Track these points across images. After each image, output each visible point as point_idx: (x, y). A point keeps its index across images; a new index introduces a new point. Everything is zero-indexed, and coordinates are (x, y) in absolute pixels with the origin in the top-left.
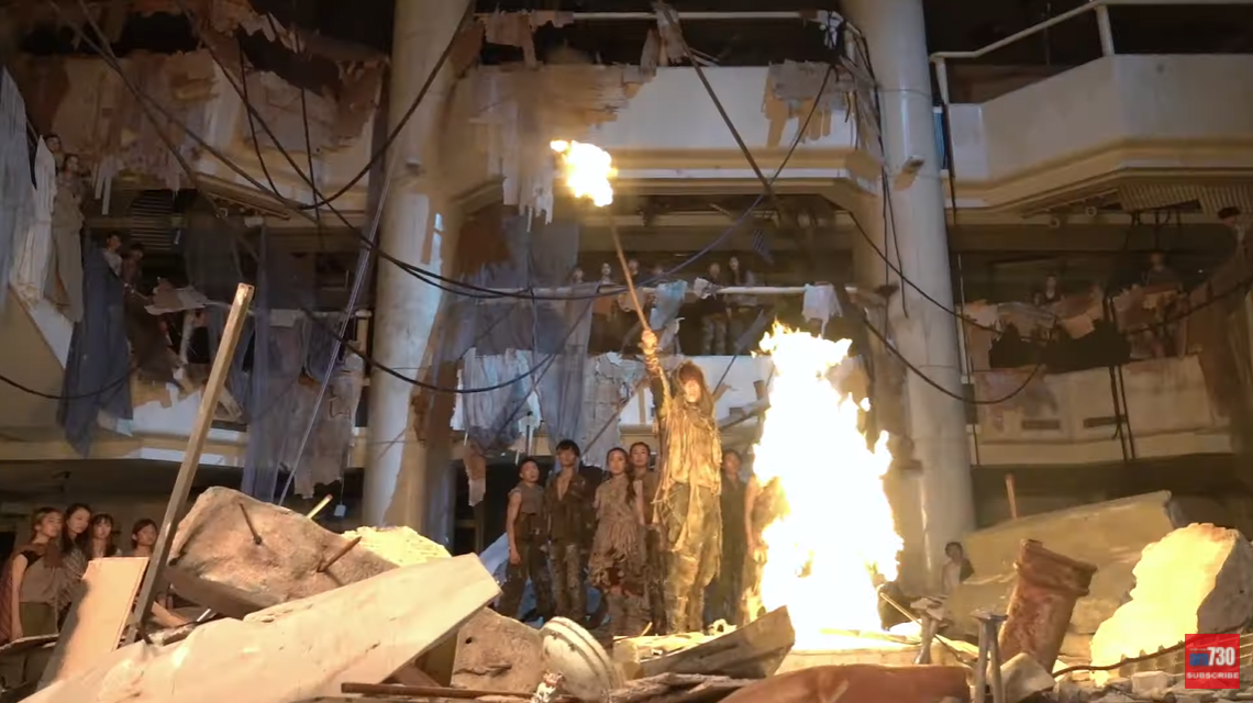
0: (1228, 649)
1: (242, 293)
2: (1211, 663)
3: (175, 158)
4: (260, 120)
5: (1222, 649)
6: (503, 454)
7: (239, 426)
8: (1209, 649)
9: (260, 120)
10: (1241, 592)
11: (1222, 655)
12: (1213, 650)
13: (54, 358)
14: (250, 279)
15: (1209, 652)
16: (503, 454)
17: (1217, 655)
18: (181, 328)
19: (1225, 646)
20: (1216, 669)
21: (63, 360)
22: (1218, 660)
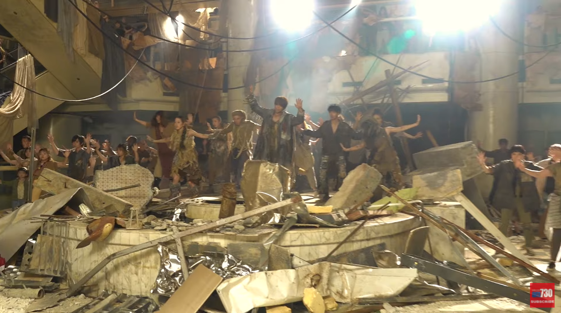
0: (550, 290)
1: (300, 169)
2: (542, 296)
3: (83, 12)
4: (73, 4)
5: (546, 290)
6: (139, 147)
7: (177, 95)
8: (541, 290)
9: (73, 4)
10: (367, 188)
11: (546, 293)
12: (542, 290)
13: (98, 76)
14: (299, 168)
15: (541, 291)
16: (139, 147)
17: (544, 292)
18: (149, 53)
19: (548, 289)
20: (543, 299)
21: (100, 75)
22: (545, 295)
